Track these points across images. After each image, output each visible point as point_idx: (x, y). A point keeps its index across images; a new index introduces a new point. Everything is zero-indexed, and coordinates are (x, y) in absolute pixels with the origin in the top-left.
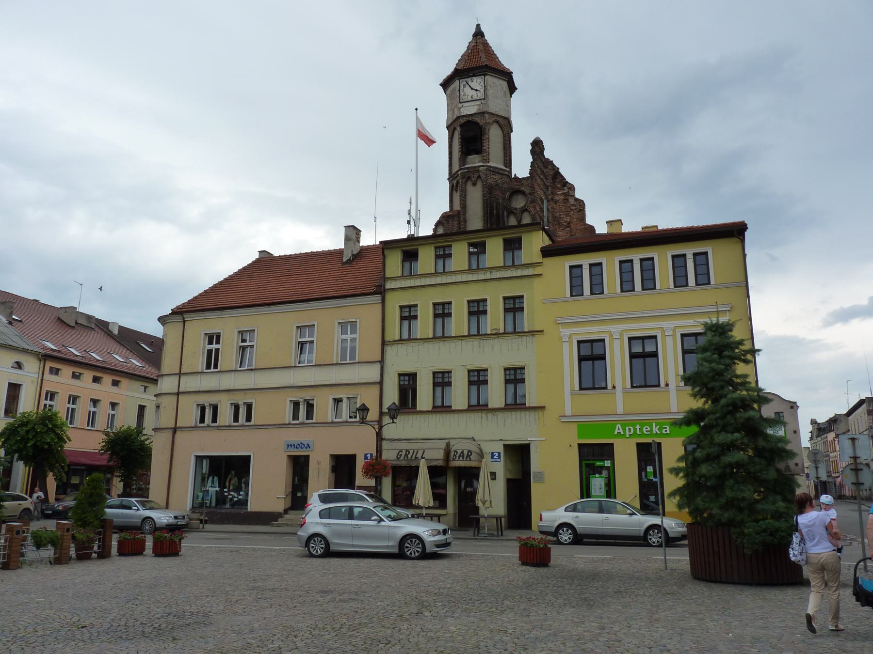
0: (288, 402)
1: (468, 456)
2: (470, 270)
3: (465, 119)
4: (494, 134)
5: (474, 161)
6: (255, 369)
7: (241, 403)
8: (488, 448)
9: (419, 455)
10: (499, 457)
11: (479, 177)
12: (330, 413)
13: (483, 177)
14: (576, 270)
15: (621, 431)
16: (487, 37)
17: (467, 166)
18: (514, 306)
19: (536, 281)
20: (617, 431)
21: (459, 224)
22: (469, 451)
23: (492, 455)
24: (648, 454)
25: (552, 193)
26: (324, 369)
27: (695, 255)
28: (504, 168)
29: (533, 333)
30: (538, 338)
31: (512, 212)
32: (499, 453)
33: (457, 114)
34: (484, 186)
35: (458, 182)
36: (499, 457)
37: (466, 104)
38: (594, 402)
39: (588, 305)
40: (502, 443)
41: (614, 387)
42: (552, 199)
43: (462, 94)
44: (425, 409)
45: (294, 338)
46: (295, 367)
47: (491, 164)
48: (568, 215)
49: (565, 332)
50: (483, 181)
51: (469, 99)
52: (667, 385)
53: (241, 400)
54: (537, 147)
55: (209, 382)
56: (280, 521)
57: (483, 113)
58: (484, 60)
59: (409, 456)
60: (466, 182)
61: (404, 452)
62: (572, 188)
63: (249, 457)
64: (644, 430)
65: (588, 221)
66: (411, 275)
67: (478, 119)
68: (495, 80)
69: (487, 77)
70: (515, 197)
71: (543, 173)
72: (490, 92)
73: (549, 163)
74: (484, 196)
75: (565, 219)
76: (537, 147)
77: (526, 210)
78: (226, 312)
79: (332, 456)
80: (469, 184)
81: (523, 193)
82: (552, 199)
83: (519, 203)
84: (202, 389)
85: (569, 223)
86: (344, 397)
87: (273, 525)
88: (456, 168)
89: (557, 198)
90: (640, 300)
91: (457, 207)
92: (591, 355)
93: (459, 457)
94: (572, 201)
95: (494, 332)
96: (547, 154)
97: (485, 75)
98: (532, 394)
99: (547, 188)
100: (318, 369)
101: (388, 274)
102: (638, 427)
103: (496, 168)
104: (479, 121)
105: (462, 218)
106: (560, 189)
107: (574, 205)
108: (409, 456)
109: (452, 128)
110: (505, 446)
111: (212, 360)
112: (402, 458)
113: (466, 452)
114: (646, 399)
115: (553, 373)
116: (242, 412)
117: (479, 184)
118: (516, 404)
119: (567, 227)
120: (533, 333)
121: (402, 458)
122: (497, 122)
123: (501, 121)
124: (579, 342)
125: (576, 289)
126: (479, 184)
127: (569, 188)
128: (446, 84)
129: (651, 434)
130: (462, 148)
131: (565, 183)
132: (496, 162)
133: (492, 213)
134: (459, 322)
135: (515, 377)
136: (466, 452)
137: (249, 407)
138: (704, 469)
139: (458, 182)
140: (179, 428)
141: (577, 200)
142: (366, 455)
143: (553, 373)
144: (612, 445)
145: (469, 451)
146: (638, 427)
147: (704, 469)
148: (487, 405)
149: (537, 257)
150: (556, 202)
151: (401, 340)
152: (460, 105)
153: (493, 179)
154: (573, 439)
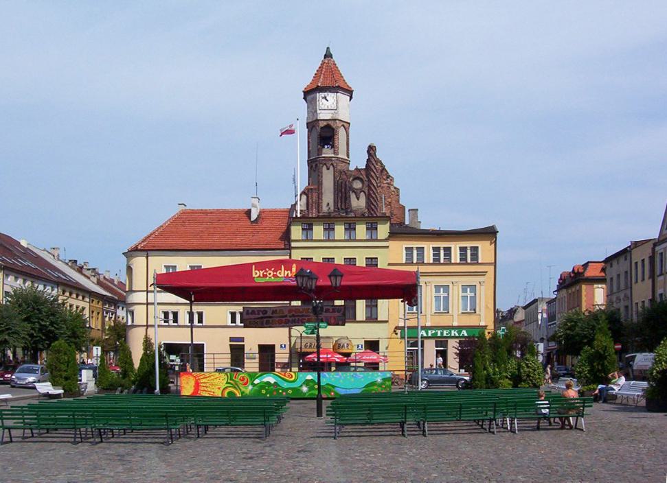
0: (228, 313)
3: (325, 123)
4: (341, 133)
5: (327, 152)
8: (355, 342)
17: (323, 155)
23: (358, 346)
28: (347, 158)
40: (363, 340)
44: (361, 320)
47: (339, 156)
48: (390, 197)
51: (326, 108)
54: (371, 150)
57: (335, 120)
63: (203, 344)
67: (331, 123)
69: (338, 94)
72: (340, 104)
76: (371, 150)
79: (259, 345)
94: (392, 189)
101: (293, 237)
104: (332, 125)
110: (365, 341)
116: (171, 316)
122: (343, 126)
123: (345, 124)
127: (391, 180)
128: (307, 94)
132: (342, 155)
148: (377, 319)
153: (341, 166)
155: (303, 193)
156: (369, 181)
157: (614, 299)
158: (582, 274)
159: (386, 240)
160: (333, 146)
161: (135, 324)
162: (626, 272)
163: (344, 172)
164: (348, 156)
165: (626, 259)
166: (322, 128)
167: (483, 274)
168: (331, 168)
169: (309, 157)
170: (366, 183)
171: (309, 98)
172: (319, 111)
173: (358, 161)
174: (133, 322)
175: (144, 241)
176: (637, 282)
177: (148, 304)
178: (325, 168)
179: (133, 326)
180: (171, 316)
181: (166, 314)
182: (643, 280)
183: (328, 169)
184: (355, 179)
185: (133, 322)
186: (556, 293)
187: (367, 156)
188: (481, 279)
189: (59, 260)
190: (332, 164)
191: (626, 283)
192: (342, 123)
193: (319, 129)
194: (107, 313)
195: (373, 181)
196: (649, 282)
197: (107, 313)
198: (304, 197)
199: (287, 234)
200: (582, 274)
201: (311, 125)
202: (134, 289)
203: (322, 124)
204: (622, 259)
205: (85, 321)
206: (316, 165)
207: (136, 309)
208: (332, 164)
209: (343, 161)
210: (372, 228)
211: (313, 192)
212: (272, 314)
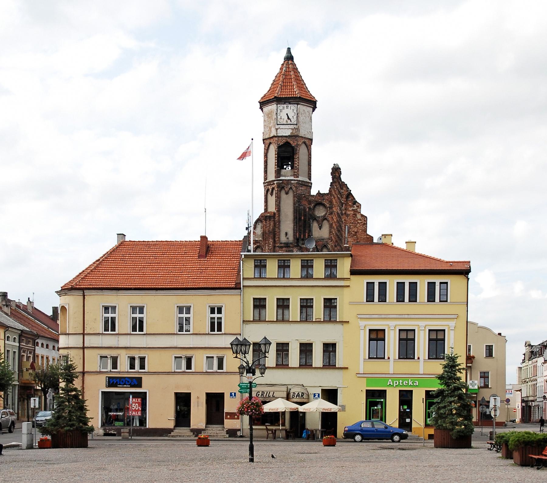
1: (302, 396)
2: (302, 278)
4: (302, 150)
6: (147, 334)
7: (137, 356)
8: (312, 391)
9: (271, 395)
10: (319, 396)
11: (291, 188)
12: (205, 365)
13: (294, 189)
14: (370, 285)
15: (391, 383)
16: (296, 60)
17: (281, 178)
18: (330, 304)
19: (346, 290)
20: (389, 383)
21: (275, 224)
22: (302, 393)
23: (315, 395)
24: (406, 398)
25: (345, 209)
26: (199, 337)
27: (441, 283)
29: (342, 322)
30: (345, 325)
31: (315, 219)
32: (319, 394)
33: (273, 133)
34: (294, 196)
35: (275, 188)
36: (319, 396)
37: (282, 127)
38: (377, 366)
39: (376, 307)
41: (389, 358)
42: (345, 213)
43: (279, 117)
45: (175, 315)
46: (177, 334)
48: (355, 227)
49: (362, 323)
50: (294, 192)
52: (419, 358)
53: (137, 355)
54: (336, 172)
55: (109, 341)
56: (172, 434)
58: (297, 92)
59: (265, 395)
60: (280, 191)
61: (261, 392)
62: (359, 206)
64: (404, 383)
65: (369, 232)
66: (260, 278)
68: (304, 108)
70: (317, 207)
71: (340, 193)
73: (343, 185)
74: (294, 204)
75: (353, 229)
76: (336, 172)
77: (326, 219)
78: (120, 292)
80: (283, 192)
81: (324, 205)
82: (345, 213)
83: (320, 212)
84: (103, 346)
85: (356, 233)
86: (215, 356)
87: (167, 436)
88: (272, 177)
89: (348, 213)
90: (407, 307)
91: (272, 208)
92: (377, 336)
93: (297, 396)
94: (359, 216)
95: (317, 320)
96: (344, 178)
97: (298, 104)
98: (340, 360)
99: (342, 204)
100: (195, 336)
102: (401, 381)
103: (303, 181)
104: (291, 142)
105: (277, 219)
106: (351, 206)
107: (360, 220)
108: (265, 395)
109: (268, 142)
111: (110, 325)
112: (260, 396)
113: (300, 394)
114: (406, 366)
115: (353, 346)
116: (137, 363)
117: (291, 194)
118: (329, 365)
119: (355, 235)
120: (342, 322)
121: (260, 396)
124: (370, 331)
125: (370, 298)
126: (291, 194)
129: (407, 385)
130: (278, 162)
131: (355, 202)
133: (300, 218)
134: (294, 311)
135: (330, 348)
136: (300, 394)
137: (142, 360)
138: (442, 411)
139: (273, 189)
140: (87, 372)
141: (362, 216)
142: (231, 393)
143: (353, 346)
144: (386, 390)
145: (302, 393)
146: (401, 381)
147: (442, 411)
149: (347, 275)
150: (348, 215)
151: (254, 321)
152: (277, 127)
154: (364, 386)
180: (137, 363)
188: (452, 323)
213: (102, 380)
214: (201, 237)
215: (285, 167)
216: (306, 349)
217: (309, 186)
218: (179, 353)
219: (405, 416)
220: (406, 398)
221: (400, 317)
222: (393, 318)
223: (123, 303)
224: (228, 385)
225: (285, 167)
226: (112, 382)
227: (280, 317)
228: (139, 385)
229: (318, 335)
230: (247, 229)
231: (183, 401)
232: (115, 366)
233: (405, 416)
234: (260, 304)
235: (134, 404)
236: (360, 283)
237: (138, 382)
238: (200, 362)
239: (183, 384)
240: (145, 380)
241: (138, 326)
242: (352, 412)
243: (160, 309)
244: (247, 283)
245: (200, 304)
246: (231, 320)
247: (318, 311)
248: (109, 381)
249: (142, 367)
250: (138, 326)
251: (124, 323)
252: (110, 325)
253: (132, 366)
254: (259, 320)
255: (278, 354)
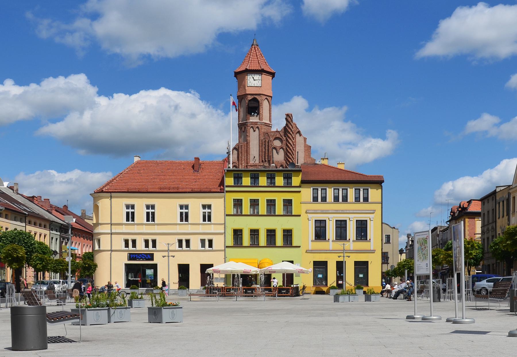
5: (254, 119)
24: (340, 266)
44: (247, 245)
53: (150, 238)
98: (295, 242)
101: (226, 184)
111: (130, 217)
116: (184, 243)
122: (267, 99)
134: (263, 208)
155: (235, 148)
156: (287, 140)
157: (490, 228)
158: (466, 209)
159: (300, 187)
160: (258, 114)
161: (101, 248)
162: (493, 209)
163: (267, 134)
164: (270, 120)
165: (493, 200)
166: (249, 101)
167: (373, 212)
168: (257, 130)
169: (239, 122)
170: (284, 142)
171: (238, 76)
172: (247, 88)
173: (278, 125)
174: (99, 247)
175: (107, 184)
176: (499, 218)
177: (111, 234)
178: (252, 130)
179: (100, 251)
180: (184, 243)
181: (180, 242)
182: (503, 216)
183: (254, 131)
184: (276, 138)
185: (99, 247)
186: (448, 223)
187: (285, 121)
189: (18, 194)
190: (258, 127)
191: (493, 217)
192: (266, 97)
193: (247, 102)
194: (63, 239)
195: (289, 140)
196: (506, 218)
197: (63, 239)
198: (236, 152)
199: (222, 183)
200: (466, 209)
201: (241, 98)
202: (100, 222)
203: (250, 98)
204: (490, 198)
205: (46, 247)
206: (245, 127)
207: (102, 237)
208: (258, 127)
209: (266, 125)
210: (288, 178)
211: (241, 149)
212: (419, 278)
213: (125, 255)
214: (195, 158)
215: (253, 114)
216: (255, 233)
217: (268, 126)
218: (203, 237)
219: (340, 276)
220: (340, 266)
221: (337, 212)
222: (331, 213)
223: (140, 204)
224: (194, 261)
225: (253, 114)
226: (132, 257)
227: (252, 213)
228: (152, 259)
229: (280, 224)
230: (227, 153)
231: (184, 270)
232: (134, 245)
233: (340, 276)
234: (238, 203)
235: (149, 272)
236: (307, 192)
237: (151, 257)
238: (195, 243)
239: (183, 258)
240: (155, 254)
241: (150, 217)
242: (305, 280)
243: (167, 207)
244: (227, 189)
245: (195, 205)
246: (217, 214)
247: (279, 208)
248: (130, 257)
249: (154, 246)
250: (150, 217)
251: (141, 214)
252: (130, 217)
253: (147, 246)
254: (239, 214)
255: (251, 238)
